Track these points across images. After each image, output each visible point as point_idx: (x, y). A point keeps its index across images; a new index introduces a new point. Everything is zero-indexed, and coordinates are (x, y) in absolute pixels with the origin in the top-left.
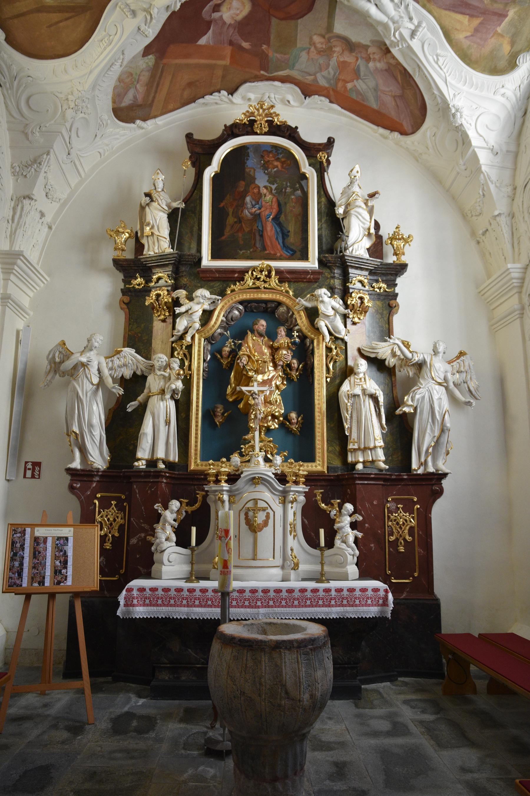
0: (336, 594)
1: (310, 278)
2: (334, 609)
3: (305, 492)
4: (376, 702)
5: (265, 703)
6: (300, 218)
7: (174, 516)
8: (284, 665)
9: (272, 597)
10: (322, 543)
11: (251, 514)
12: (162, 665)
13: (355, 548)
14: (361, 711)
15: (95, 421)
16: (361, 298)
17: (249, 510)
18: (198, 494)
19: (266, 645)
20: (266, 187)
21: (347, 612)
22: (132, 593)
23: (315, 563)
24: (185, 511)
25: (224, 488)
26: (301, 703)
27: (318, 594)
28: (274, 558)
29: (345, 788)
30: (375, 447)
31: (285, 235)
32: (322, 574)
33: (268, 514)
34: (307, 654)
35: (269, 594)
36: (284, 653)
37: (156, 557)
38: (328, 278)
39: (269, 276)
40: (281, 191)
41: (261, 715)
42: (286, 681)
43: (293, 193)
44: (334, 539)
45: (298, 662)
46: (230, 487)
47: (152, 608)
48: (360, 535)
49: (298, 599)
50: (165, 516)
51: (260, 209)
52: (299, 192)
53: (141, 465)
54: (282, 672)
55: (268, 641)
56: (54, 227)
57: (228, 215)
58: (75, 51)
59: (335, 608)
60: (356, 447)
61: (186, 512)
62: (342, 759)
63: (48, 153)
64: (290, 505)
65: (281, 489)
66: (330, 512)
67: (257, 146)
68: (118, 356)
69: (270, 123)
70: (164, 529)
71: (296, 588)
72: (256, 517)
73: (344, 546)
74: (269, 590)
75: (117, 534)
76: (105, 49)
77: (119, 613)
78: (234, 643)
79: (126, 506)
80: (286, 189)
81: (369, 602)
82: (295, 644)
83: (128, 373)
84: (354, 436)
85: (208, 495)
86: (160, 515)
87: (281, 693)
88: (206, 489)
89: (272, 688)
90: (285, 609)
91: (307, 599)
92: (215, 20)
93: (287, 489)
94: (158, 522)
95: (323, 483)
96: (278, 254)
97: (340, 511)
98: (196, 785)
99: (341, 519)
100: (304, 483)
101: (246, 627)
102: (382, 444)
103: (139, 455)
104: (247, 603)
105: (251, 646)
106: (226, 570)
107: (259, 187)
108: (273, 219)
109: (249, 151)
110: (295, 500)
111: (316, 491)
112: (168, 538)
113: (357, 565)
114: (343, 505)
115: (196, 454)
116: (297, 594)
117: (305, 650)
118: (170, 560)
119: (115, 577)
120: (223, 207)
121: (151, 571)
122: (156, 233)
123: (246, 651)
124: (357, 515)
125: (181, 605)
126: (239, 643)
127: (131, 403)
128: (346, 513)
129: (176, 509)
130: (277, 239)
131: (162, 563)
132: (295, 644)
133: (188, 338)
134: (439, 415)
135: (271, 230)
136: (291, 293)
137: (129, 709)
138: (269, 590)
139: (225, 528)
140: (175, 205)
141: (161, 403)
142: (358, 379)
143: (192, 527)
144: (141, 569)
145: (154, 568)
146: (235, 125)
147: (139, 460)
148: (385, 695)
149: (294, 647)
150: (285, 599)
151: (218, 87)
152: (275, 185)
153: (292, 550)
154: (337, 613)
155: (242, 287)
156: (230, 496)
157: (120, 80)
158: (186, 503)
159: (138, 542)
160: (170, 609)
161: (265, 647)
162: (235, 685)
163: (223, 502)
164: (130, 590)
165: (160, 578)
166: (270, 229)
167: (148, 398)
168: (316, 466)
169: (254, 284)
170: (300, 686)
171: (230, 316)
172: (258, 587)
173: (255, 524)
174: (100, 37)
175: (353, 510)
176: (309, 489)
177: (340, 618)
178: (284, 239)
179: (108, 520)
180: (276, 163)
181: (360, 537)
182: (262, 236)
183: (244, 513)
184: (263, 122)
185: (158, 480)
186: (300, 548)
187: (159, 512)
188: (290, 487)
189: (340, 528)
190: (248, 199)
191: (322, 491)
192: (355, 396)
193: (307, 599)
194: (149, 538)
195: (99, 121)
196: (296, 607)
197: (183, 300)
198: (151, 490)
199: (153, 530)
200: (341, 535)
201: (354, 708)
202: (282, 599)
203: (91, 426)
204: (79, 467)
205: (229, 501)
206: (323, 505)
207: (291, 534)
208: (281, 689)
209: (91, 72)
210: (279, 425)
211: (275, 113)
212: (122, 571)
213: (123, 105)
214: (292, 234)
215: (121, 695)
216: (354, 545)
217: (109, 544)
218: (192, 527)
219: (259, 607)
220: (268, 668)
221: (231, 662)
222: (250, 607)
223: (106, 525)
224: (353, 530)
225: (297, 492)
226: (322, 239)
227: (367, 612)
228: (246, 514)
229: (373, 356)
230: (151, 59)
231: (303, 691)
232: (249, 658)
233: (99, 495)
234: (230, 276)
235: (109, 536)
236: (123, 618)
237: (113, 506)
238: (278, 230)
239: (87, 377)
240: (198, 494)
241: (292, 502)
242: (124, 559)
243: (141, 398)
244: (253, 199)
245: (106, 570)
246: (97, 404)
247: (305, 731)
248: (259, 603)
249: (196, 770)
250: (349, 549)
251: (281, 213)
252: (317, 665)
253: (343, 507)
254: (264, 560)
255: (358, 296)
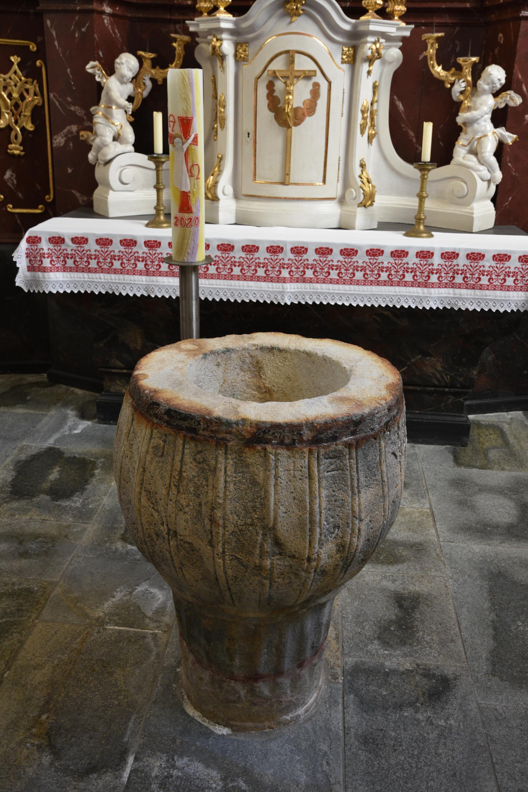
0: (442, 262)
2: (435, 292)
3: (404, 39)
4: (493, 454)
5: (224, 560)
7: (129, 88)
8: (272, 482)
9: (311, 262)
10: (426, 155)
11: (279, 85)
12: (114, 371)
13: (496, 165)
14: (464, 471)
17: (276, 77)
18: (175, 40)
19: (230, 433)
21: (461, 299)
22: (40, 246)
23: (408, 194)
24: (152, 79)
25: (223, 25)
26: (314, 564)
27: (405, 260)
28: (324, 181)
29: (408, 666)
32: (419, 220)
33: (316, 86)
34: (337, 456)
35: (305, 257)
36: (276, 455)
37: (98, 173)
41: (217, 579)
42: (275, 519)
44: (453, 146)
45: (310, 477)
46: (236, 23)
47: (80, 275)
48: (510, 138)
49: (363, 269)
50: (109, 89)
54: (266, 498)
55: (237, 423)
59: (437, 290)
62: (411, 588)
64: (365, 67)
65: (347, 27)
66: (452, 84)
70: (108, 117)
71: (361, 247)
72: (289, 93)
73: (472, 160)
74: (306, 249)
75: (30, 127)
77: (19, 281)
78: (156, 416)
79: (40, 68)
81: (510, 281)
82: (307, 434)
85: (197, 43)
86: (100, 87)
87: (262, 546)
88: (192, 29)
89: (241, 531)
90: (336, 286)
91: (381, 269)
93: (362, 28)
94: (97, 102)
95: (447, 20)
97: (474, 85)
98: (120, 632)
99: (475, 103)
100: (401, 18)
101: (210, 358)
104: (261, 272)
106: (186, 216)
110: (377, 55)
111: (425, 36)
112: (119, 135)
113: (494, 200)
114: (483, 69)
116: (361, 259)
117: (333, 447)
118: (125, 180)
119: (36, 208)
121: (92, 200)
123: (180, 441)
124: (511, 92)
125: (134, 272)
126: (166, 417)
128: (486, 87)
131: (108, 186)
132: (307, 434)
137: (56, 441)
138: (306, 249)
139: (182, 115)
143: (155, 113)
144: (78, 195)
145: (97, 194)
148: (511, 440)
149: (301, 441)
150: (338, 268)
153: (362, 166)
154: (441, 299)
156: (237, 45)
158: (152, 59)
159: (67, 142)
160: (114, 277)
161: (228, 436)
162: (157, 511)
163: (223, 58)
164: (34, 241)
165: (104, 216)
170: (311, 530)
172: (285, 242)
173: (288, 110)
175: (503, 81)
176: (412, 32)
177: (445, 308)
179: (10, 96)
181: (510, 142)
183: (266, 83)
185: (90, 7)
186: (382, 163)
187: (98, 79)
188: (368, 22)
189: (468, 123)
191: (440, 34)
193: (381, 269)
194: (84, 134)
196: (358, 283)
198: (80, 30)
199: (90, 117)
200: (469, 136)
201: (452, 463)
202: (331, 267)
205: (236, 56)
206: (439, 69)
207: (362, 133)
208: (264, 535)
212: (49, 198)
215: (53, 412)
216: (493, 160)
217: (18, 146)
218: (155, 113)
219: (284, 280)
220: (231, 487)
221: (149, 458)
222: (267, 279)
223: (7, 107)
224: (496, 127)
225: (383, 35)
227: (502, 302)
228: (270, 86)
231: (320, 540)
232: (188, 459)
235: (16, 131)
236: (29, 291)
237: (15, 67)
240: (175, 40)
241: (370, 61)
242: (51, 176)
245: (20, 195)
247: (323, 600)
248: (285, 273)
249: (131, 593)
250: (482, 168)
252: (362, 479)
253: (484, 75)
254: (304, 184)
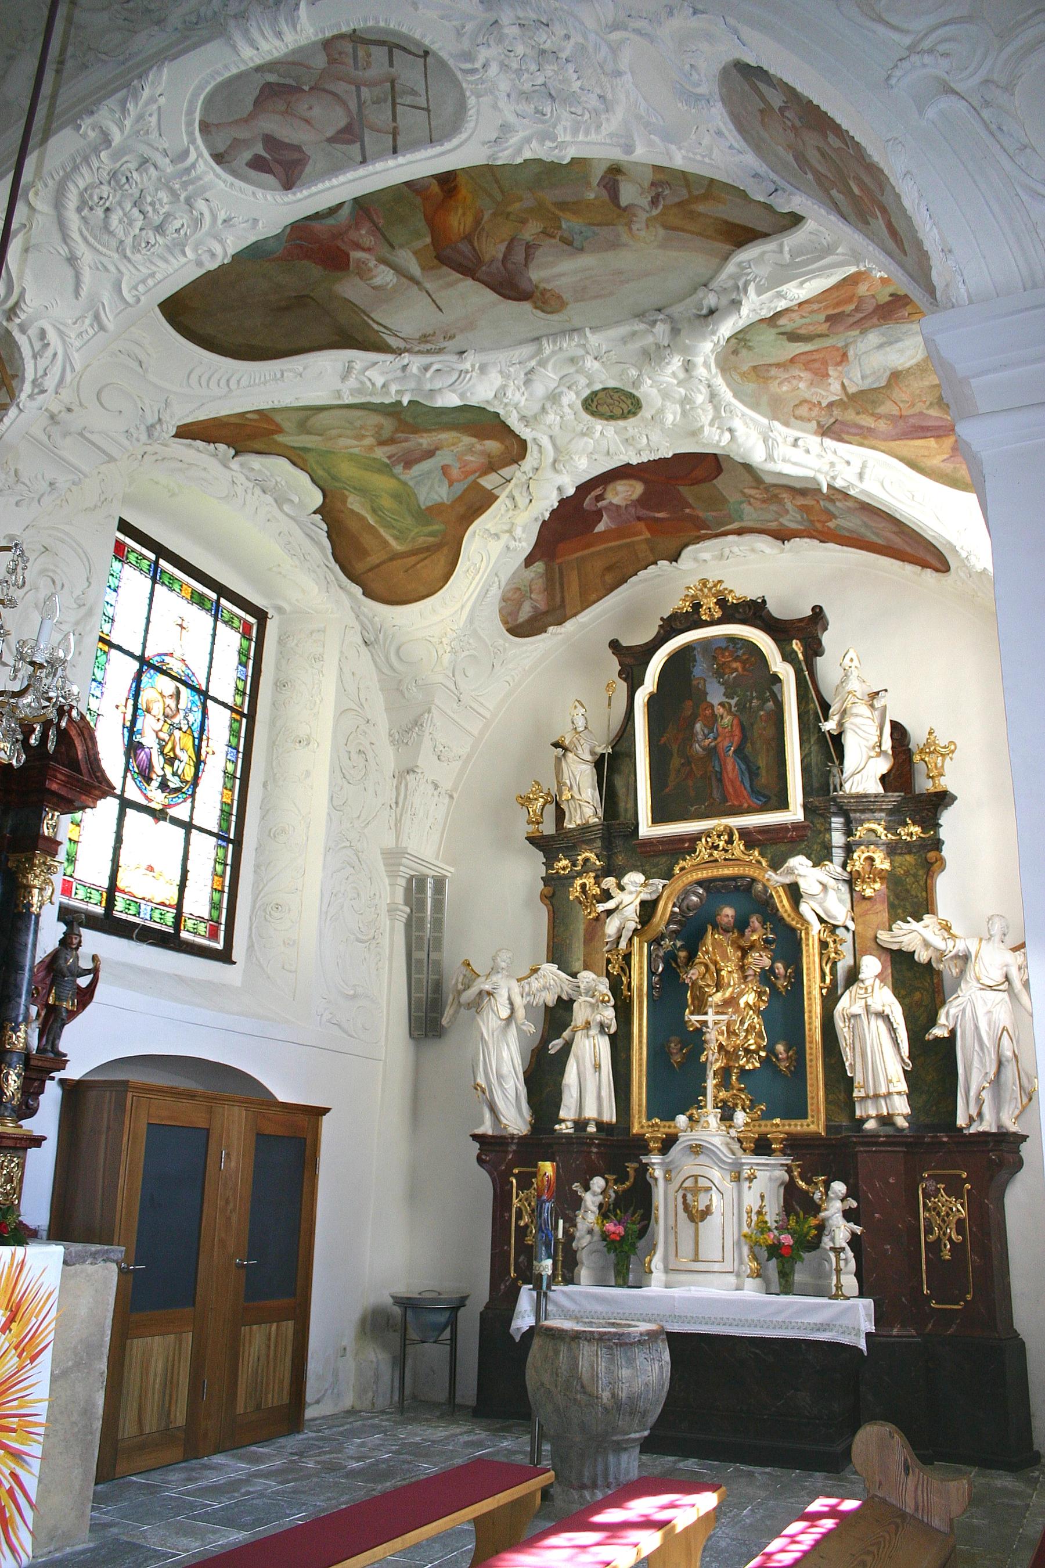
1: (792, 837)
6: (773, 744)
11: (689, 1197)
15: (507, 1069)
16: (871, 859)
20: (722, 704)
30: (890, 1094)
31: (753, 773)
34: (610, 1348)
38: (820, 832)
39: (730, 841)
40: (745, 706)
43: (761, 707)
48: (858, 1230)
51: (715, 739)
52: (770, 704)
53: (565, 1128)
56: (455, 796)
57: (672, 755)
58: (441, 588)
60: (863, 1094)
61: (615, 1192)
63: (429, 712)
67: (706, 644)
68: (535, 975)
69: (722, 603)
76: (473, 579)
80: (751, 703)
83: (551, 999)
84: (859, 1079)
92: (605, 508)
96: (745, 805)
97: (827, 1195)
102: (903, 1087)
103: (562, 1114)
105: (553, 1335)
107: (712, 706)
108: (735, 752)
109: (696, 652)
115: (640, 1112)
120: (665, 744)
122: (577, 796)
127: (554, 1042)
129: (599, 1191)
130: (742, 782)
133: (623, 944)
134: (989, 1039)
135: (733, 770)
136: (764, 864)
140: (600, 750)
141: (587, 1042)
142: (861, 988)
146: (674, 616)
147: (564, 1121)
151: (652, 559)
152: (736, 699)
155: (695, 862)
157: (504, 599)
166: (732, 768)
167: (574, 1032)
168: (808, 1125)
169: (711, 855)
171: (685, 905)
174: (465, 569)
178: (751, 780)
179: (529, 1205)
180: (735, 665)
182: (720, 780)
184: (712, 605)
190: (698, 726)
192: (856, 1016)
195: (492, 649)
197: (614, 891)
203: (500, 1077)
204: (490, 1132)
209: (463, 607)
210: (761, 1063)
211: (726, 589)
213: (521, 620)
214: (763, 772)
226: (810, 771)
228: (684, 1197)
229: (895, 947)
230: (539, 566)
233: (516, 1171)
234: (680, 846)
238: (743, 767)
239: (493, 1011)
243: (566, 1034)
244: (705, 725)
246: (508, 1045)
251: (746, 742)
255: (863, 857)
